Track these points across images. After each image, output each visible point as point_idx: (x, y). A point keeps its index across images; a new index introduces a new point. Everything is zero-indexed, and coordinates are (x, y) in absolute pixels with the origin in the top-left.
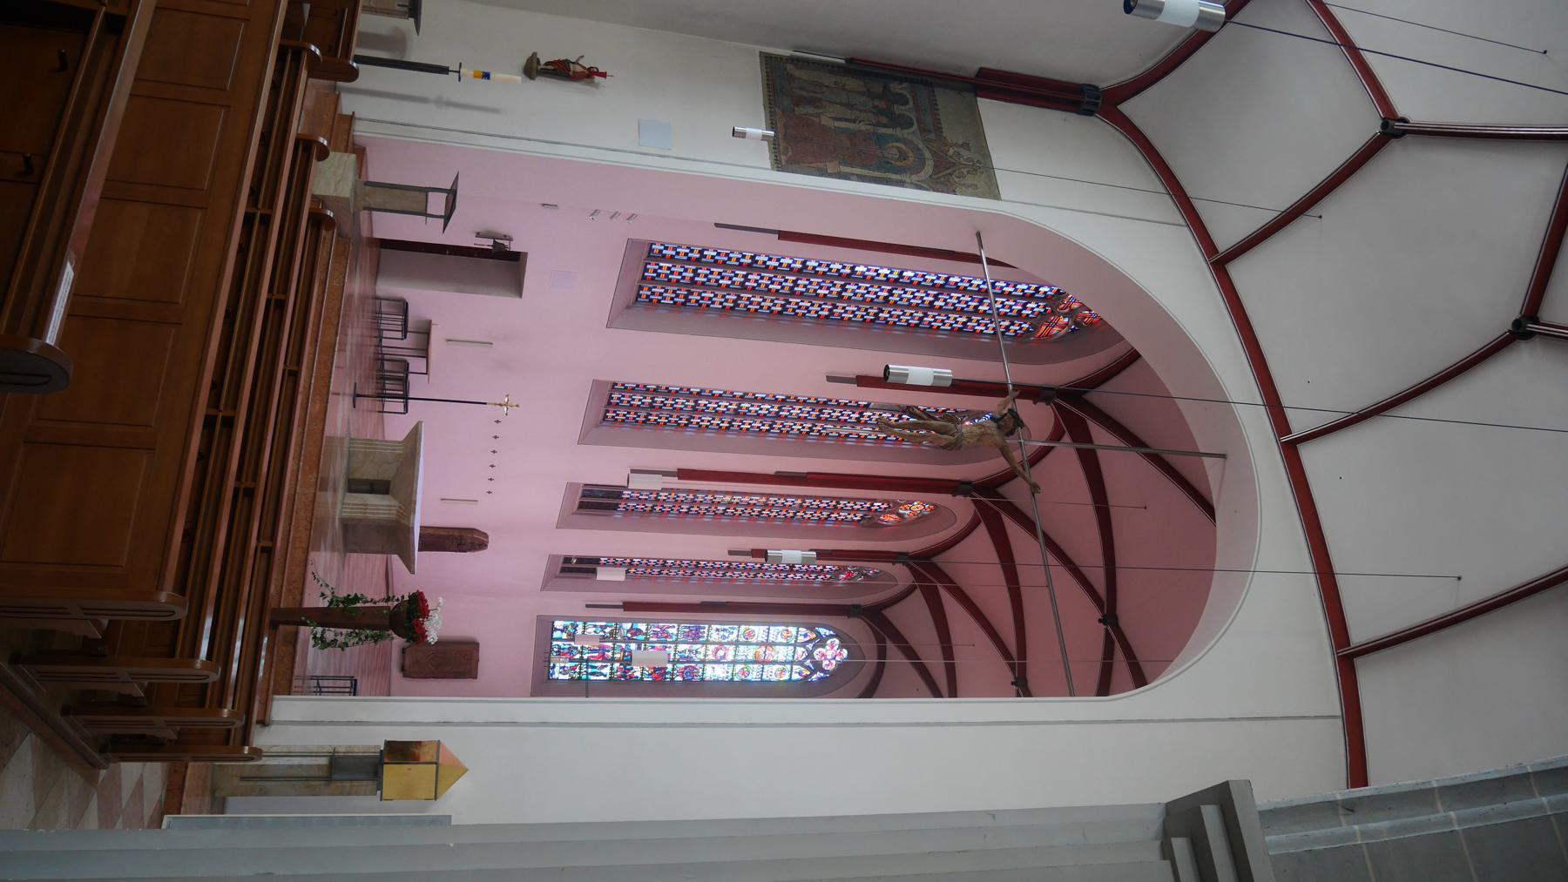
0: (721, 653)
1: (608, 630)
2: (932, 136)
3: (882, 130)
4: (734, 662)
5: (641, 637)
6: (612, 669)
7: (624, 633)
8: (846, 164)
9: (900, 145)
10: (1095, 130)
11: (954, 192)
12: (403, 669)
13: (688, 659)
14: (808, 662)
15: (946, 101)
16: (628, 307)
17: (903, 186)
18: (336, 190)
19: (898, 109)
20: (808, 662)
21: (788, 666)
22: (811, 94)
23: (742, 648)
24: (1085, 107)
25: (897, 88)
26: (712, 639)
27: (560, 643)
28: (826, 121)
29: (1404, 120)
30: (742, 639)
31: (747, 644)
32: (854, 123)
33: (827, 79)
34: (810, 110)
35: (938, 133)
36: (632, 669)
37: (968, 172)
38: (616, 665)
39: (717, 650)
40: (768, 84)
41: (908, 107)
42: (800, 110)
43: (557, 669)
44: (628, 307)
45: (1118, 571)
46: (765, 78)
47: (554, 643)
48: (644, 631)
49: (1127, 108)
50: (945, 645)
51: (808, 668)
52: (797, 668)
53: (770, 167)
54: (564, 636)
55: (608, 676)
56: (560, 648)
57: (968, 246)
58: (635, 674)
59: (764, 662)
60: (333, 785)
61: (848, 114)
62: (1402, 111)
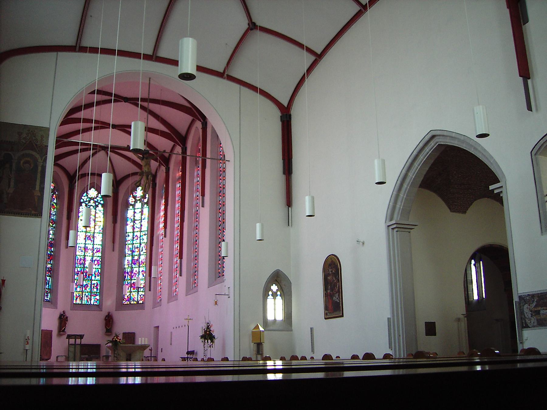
9: (22, 162)
16: (208, 327)
24: (288, 119)
28: (11, 191)
29: (249, 24)
36: (48, 268)
44: (208, 327)
45: (55, 54)
49: (285, 103)
50: (101, 103)
58: (50, 267)
62: (247, 26)
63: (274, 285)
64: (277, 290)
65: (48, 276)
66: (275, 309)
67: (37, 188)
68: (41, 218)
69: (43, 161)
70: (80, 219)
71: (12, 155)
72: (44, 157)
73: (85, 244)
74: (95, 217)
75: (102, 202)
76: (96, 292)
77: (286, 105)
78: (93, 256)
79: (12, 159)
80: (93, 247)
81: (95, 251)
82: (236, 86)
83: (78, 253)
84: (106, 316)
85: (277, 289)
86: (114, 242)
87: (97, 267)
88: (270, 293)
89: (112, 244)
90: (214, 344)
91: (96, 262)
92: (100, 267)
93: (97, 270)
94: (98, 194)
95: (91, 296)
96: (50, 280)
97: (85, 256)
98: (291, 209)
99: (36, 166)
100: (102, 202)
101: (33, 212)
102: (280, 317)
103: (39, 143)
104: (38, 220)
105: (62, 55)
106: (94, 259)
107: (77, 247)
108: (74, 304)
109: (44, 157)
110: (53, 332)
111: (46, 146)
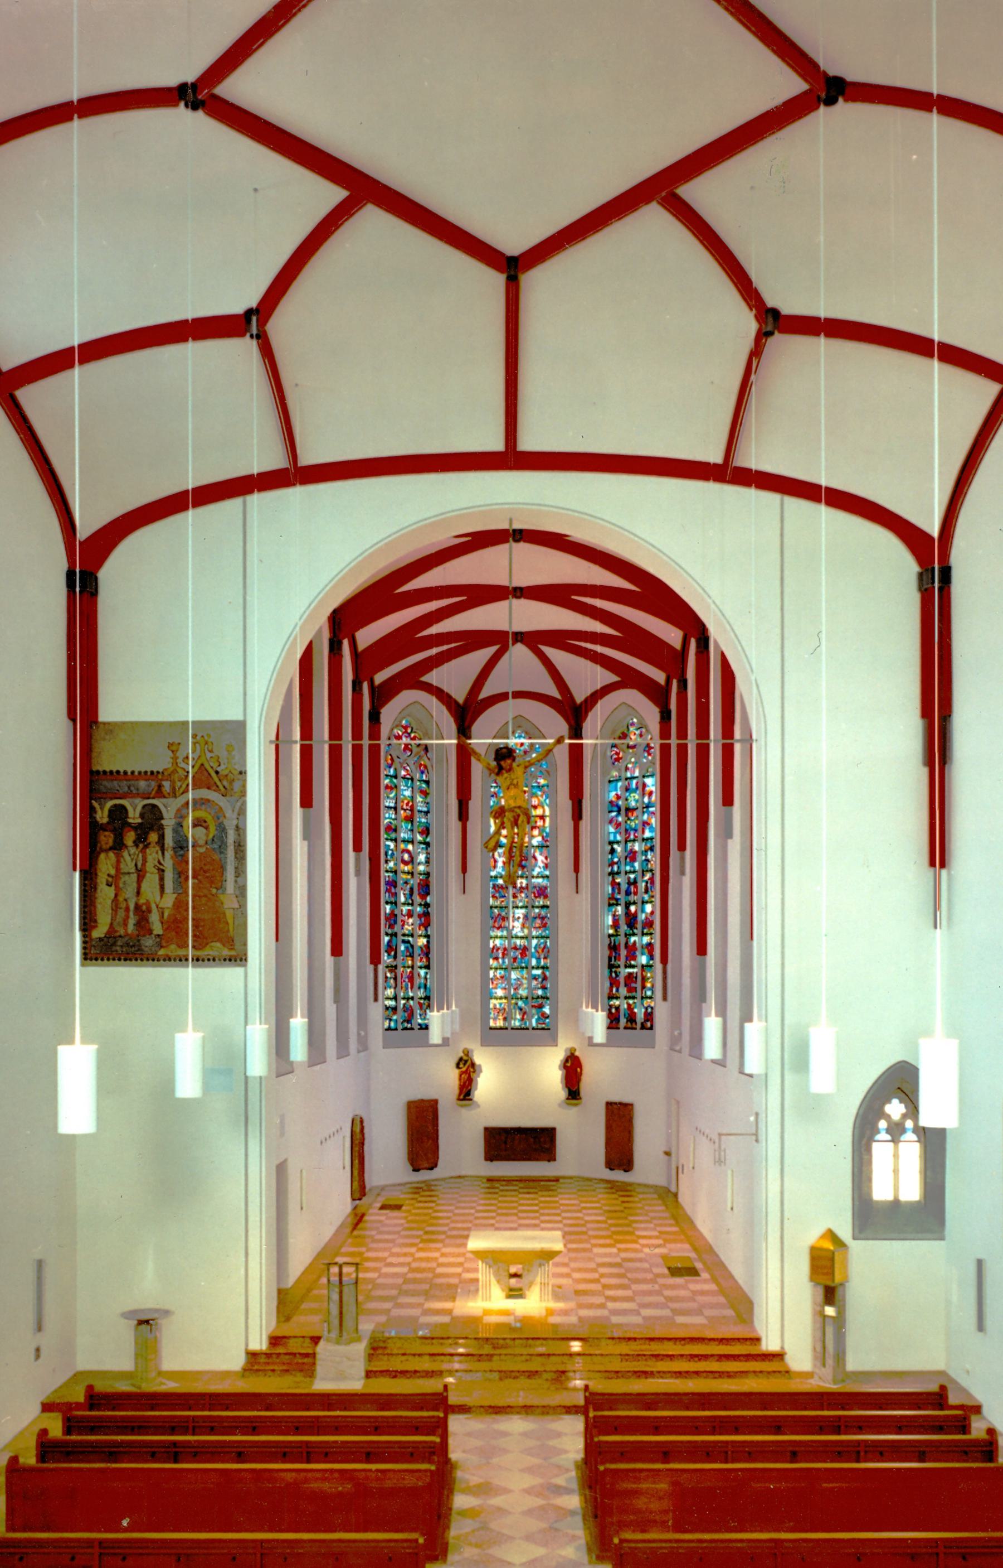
1: (389, 975)
2: (167, 785)
3: (169, 841)
11: (243, 773)
12: (431, 1169)
17: (245, 830)
18: (568, 1491)
19: (134, 816)
22: (131, 914)
32: (163, 871)
34: (154, 918)
35: (160, 777)
37: (211, 751)
40: (125, 960)
42: (157, 928)
57: (273, 747)
63: (895, 1101)
64: (904, 1116)
65: (421, 968)
68: (245, 966)
72: (239, 804)
77: (934, 530)
79: (162, 818)
82: (771, 499)
84: (567, 1060)
86: (577, 869)
88: (883, 1124)
89: (574, 875)
98: (949, 874)
102: (911, 1191)
103: (223, 767)
104: (239, 971)
105: (256, 500)
108: (491, 1028)
109: (239, 804)
111: (241, 773)
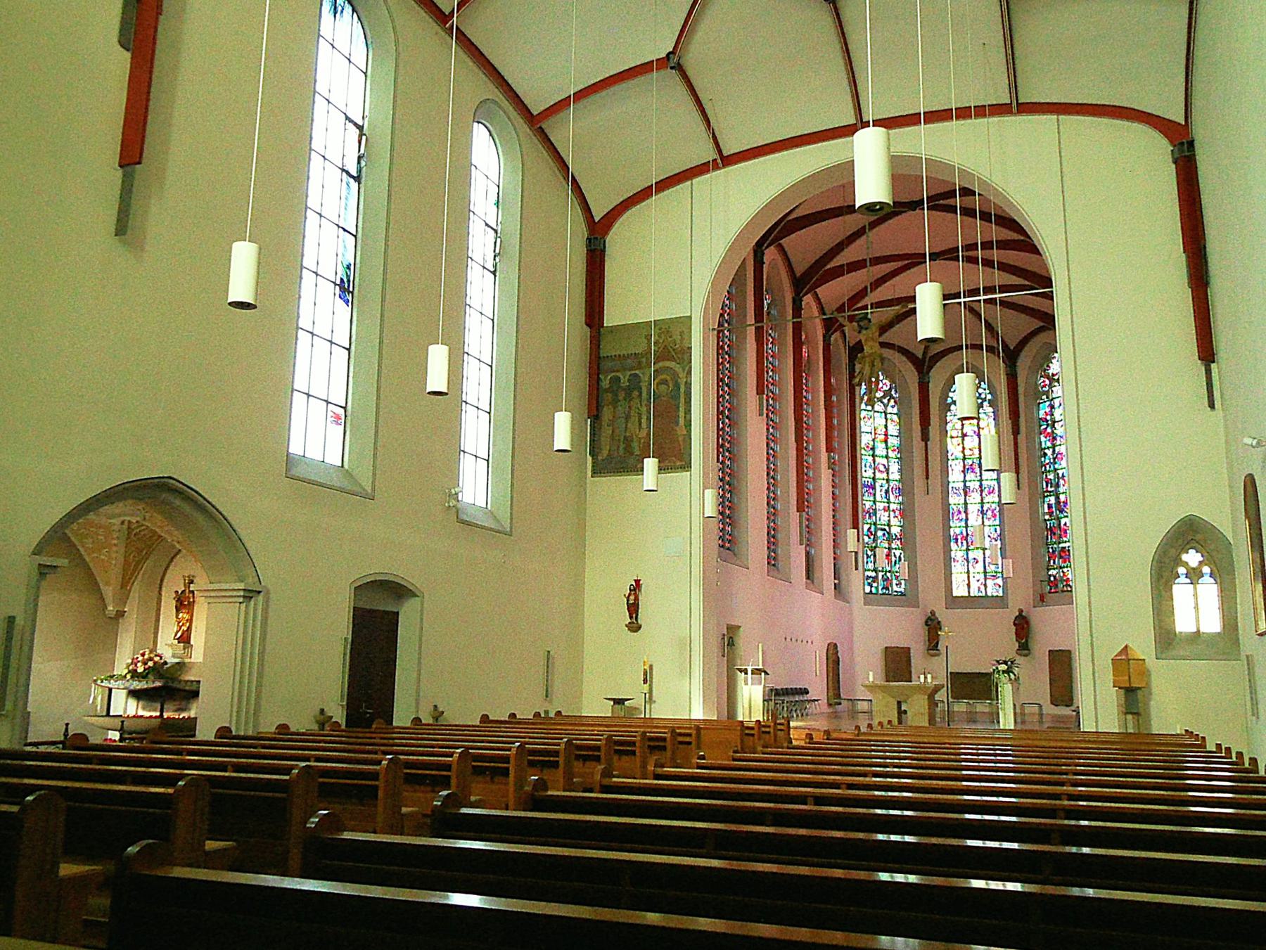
0: (882, 468)
4: (887, 457)
5: (873, 529)
6: (896, 549)
7: (871, 540)
8: (677, 423)
10: (616, 240)
13: (887, 492)
14: (885, 401)
15: (607, 349)
19: (624, 382)
20: (885, 401)
21: (889, 416)
23: (877, 453)
25: (605, 383)
26: (872, 475)
27: (880, 588)
30: (871, 452)
31: (873, 449)
33: (607, 431)
34: (635, 444)
37: (670, 337)
38: (893, 546)
39: (879, 471)
41: (622, 377)
43: (898, 589)
46: (626, 474)
47: (880, 592)
48: (869, 526)
51: (889, 400)
52: (889, 410)
53: (689, 473)
54: (875, 585)
55: (900, 551)
56: (883, 588)
59: (886, 435)
60: (1141, 710)
61: (635, 419)
66: (1196, 607)
67: (682, 421)
69: (687, 374)
70: (949, 435)
71: (641, 375)
72: (687, 368)
73: (965, 481)
74: (979, 428)
75: (989, 397)
76: (996, 572)
78: (982, 503)
80: (981, 486)
81: (986, 491)
83: (951, 501)
85: (1201, 559)
87: (991, 523)
90: (679, 728)
91: (989, 513)
92: (997, 522)
93: (993, 528)
94: (980, 383)
95: (986, 579)
96: (902, 556)
97: (966, 504)
99: (677, 386)
100: (989, 397)
101: (678, 463)
106: (985, 509)
107: (950, 489)
110: (912, 651)
